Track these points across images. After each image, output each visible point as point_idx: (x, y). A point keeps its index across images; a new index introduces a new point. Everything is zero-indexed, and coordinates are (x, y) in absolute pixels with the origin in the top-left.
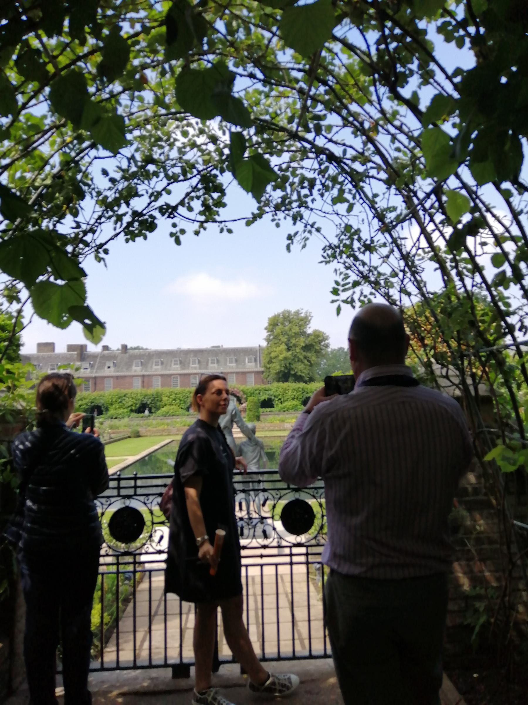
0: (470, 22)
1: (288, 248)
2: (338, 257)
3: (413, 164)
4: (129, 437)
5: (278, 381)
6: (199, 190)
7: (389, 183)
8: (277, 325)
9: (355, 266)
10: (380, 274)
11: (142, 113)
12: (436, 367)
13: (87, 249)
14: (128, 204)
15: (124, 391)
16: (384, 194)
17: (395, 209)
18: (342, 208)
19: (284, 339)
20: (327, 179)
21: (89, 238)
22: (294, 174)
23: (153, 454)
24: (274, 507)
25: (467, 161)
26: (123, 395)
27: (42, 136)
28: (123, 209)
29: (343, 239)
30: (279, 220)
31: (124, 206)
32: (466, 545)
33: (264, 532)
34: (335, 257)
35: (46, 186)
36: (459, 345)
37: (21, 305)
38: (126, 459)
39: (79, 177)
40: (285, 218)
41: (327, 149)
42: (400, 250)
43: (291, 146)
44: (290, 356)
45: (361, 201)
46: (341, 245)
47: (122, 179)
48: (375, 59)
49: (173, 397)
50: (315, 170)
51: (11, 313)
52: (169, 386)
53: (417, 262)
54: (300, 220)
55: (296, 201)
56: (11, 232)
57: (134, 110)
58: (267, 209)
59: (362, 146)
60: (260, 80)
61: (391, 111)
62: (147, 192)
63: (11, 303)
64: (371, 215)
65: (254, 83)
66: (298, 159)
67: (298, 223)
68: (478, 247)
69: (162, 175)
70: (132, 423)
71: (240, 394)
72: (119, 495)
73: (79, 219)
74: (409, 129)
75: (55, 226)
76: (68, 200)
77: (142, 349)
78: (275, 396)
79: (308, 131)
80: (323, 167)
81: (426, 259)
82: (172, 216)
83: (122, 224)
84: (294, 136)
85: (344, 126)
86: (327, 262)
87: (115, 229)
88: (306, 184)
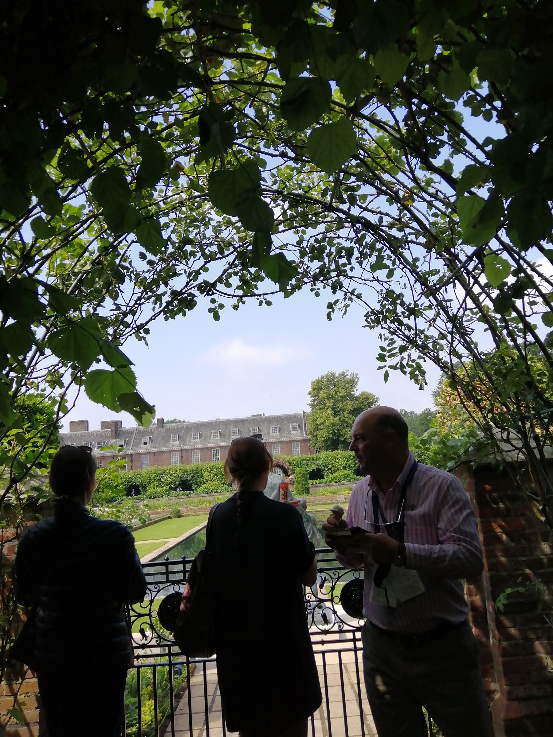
0: (495, 97)
1: (329, 317)
2: (383, 323)
3: (452, 229)
4: (170, 518)
5: (327, 450)
6: (236, 266)
7: (428, 246)
8: (322, 389)
9: (400, 330)
10: (427, 337)
11: (177, 196)
12: (496, 430)
13: (128, 330)
14: (166, 284)
15: (162, 468)
16: (424, 257)
17: (437, 272)
18: (382, 274)
19: (330, 403)
20: (364, 247)
21: (129, 319)
22: (331, 244)
23: (196, 535)
24: (333, 588)
25: (506, 225)
26: (161, 472)
27: (81, 226)
28: (162, 289)
29: (385, 304)
30: (319, 289)
31: (162, 287)
32: (547, 622)
33: (324, 616)
34: (379, 323)
35: (86, 272)
36: (518, 407)
37: (64, 389)
38: (168, 542)
39: (117, 261)
40: (324, 287)
41: (363, 218)
42: (446, 313)
43: (326, 216)
44: (338, 422)
45: (401, 266)
46: (384, 310)
47: (159, 261)
48: (404, 131)
49: (214, 471)
50: (351, 240)
51: (54, 397)
52: (209, 460)
53: (465, 324)
54: (340, 289)
55: (334, 271)
56: (52, 319)
57: (169, 194)
58: (306, 280)
59: (398, 213)
60: (291, 158)
61: (424, 179)
62: (185, 272)
63: (54, 388)
64: (412, 279)
65: (286, 161)
66: (334, 229)
67: (338, 291)
68: (527, 307)
69: (199, 254)
70: (172, 501)
71: (286, 466)
72: (167, 581)
73: (120, 301)
74: (445, 196)
75: (95, 309)
76: (108, 284)
77: (179, 422)
78: (324, 466)
79: (343, 202)
80: (359, 235)
81: (475, 319)
82: (210, 293)
83: (161, 304)
84: (329, 208)
85: (378, 194)
86: (371, 327)
87: (154, 309)
88: (343, 254)
